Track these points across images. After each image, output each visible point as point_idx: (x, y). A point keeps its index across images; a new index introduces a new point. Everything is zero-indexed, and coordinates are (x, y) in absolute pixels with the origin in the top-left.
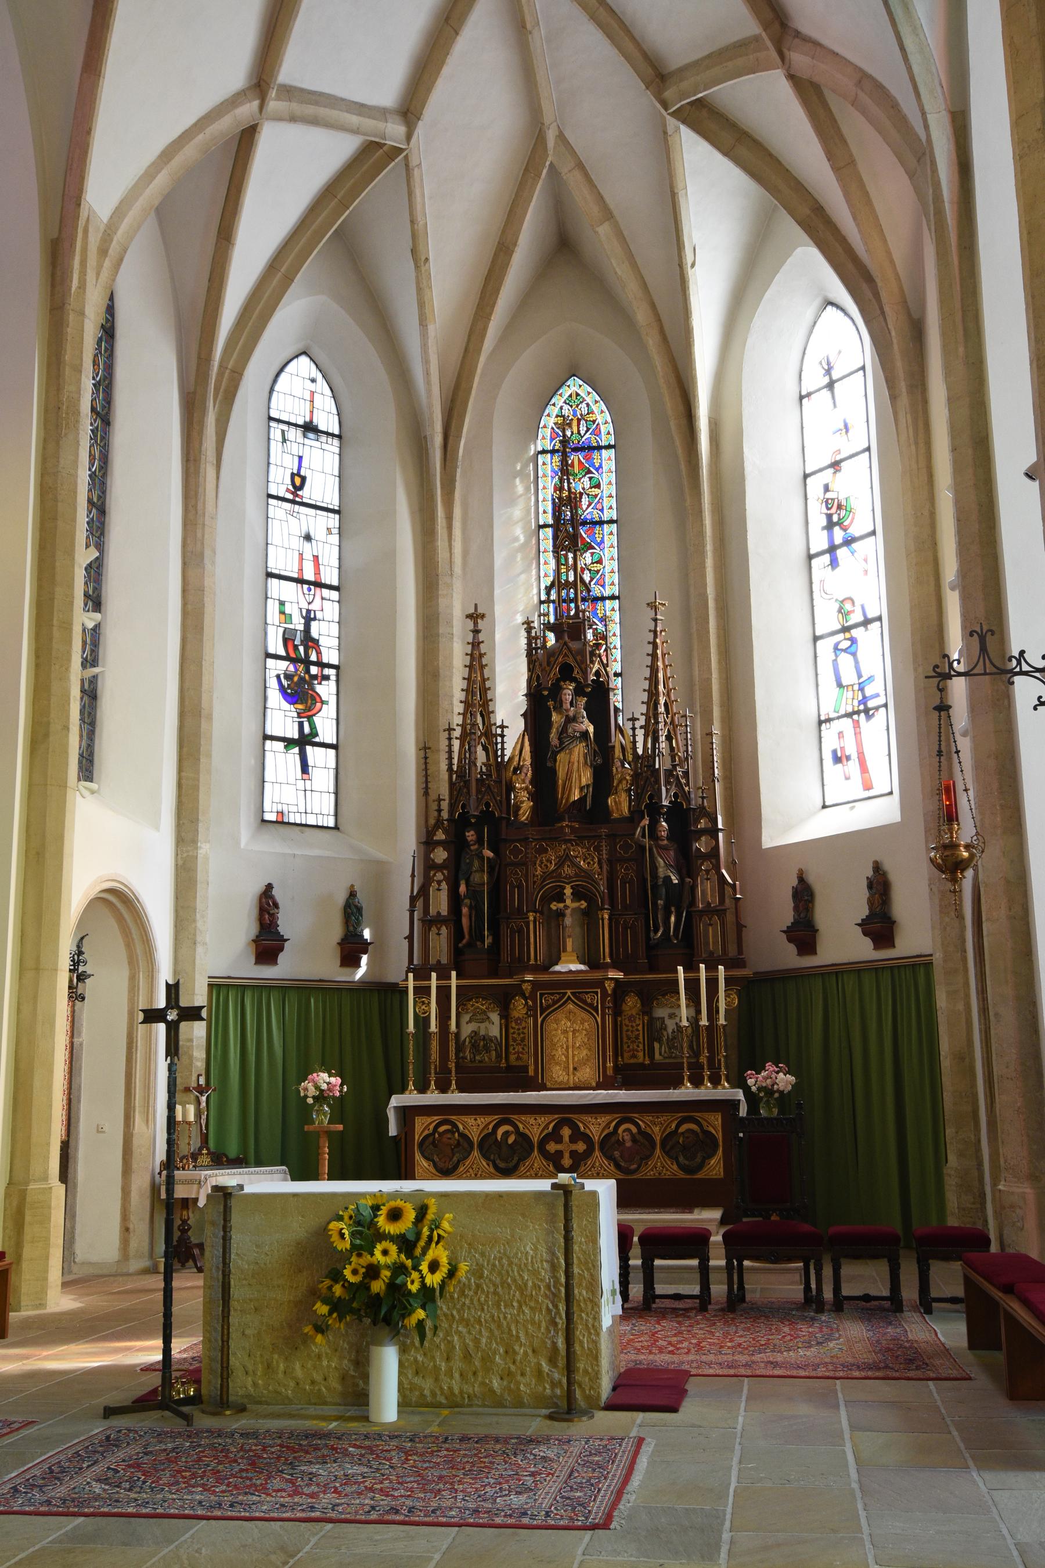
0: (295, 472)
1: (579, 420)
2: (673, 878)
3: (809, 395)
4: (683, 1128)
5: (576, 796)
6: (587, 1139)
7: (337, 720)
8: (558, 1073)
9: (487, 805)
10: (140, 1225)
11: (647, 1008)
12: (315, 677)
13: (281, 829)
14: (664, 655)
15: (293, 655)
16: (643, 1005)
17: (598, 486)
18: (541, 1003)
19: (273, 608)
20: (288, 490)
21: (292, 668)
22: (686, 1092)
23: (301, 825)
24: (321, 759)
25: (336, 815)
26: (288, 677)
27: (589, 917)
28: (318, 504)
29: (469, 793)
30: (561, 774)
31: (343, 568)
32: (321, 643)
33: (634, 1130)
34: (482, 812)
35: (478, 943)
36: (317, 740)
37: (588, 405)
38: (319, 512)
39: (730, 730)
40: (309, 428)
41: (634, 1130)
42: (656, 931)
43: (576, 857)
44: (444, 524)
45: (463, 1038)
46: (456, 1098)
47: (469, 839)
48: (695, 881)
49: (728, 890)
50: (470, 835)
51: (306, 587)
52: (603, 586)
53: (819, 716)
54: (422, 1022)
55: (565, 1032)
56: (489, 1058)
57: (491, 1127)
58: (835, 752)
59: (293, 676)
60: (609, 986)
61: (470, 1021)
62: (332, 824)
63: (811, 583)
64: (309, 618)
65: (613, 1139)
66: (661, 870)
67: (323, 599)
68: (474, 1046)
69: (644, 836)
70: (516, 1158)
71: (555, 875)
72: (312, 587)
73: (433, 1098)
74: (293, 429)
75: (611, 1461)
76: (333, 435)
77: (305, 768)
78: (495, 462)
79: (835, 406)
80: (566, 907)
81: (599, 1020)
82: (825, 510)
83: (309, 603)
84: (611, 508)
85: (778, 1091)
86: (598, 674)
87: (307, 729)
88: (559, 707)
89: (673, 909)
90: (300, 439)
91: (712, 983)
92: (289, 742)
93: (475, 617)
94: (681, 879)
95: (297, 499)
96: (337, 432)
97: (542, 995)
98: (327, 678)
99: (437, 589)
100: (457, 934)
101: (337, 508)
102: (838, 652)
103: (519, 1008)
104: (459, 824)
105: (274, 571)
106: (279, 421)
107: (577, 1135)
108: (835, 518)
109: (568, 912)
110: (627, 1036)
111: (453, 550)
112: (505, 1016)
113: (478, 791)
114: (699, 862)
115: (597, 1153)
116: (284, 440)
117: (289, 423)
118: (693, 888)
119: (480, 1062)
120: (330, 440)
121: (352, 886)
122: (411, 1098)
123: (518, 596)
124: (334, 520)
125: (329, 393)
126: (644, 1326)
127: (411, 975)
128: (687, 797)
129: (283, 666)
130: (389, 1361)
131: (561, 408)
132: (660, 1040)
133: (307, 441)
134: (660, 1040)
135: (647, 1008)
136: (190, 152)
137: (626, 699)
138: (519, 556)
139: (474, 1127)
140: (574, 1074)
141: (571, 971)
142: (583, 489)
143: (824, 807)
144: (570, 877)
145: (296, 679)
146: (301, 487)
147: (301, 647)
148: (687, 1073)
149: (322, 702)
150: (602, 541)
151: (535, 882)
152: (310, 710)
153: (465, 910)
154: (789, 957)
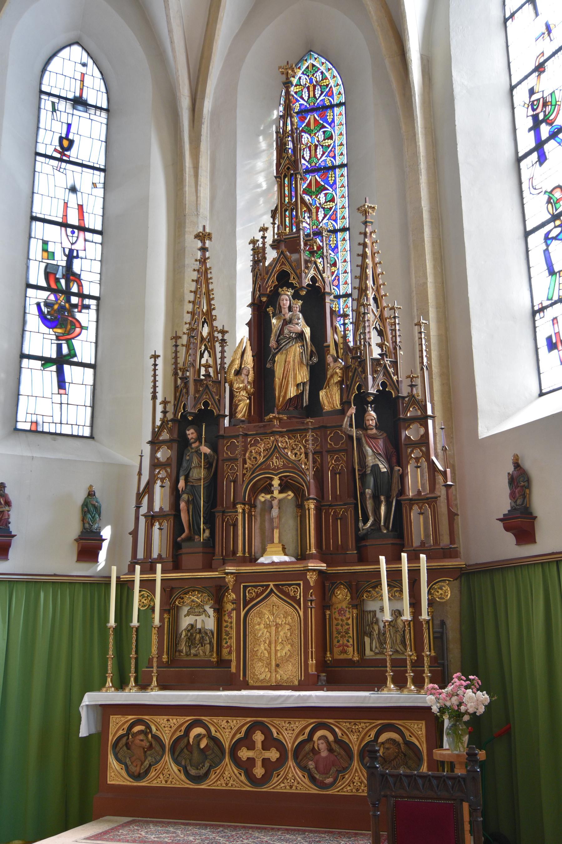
0: (64, 135)
1: (314, 87)
2: (381, 466)
3: (512, 16)
4: (383, 737)
5: (292, 392)
6: (280, 746)
7: (96, 343)
8: (260, 671)
9: (206, 404)
11: (357, 602)
12: (76, 306)
13: (32, 437)
14: (373, 254)
15: (53, 286)
16: (352, 598)
17: (331, 138)
18: (245, 596)
19: (36, 248)
20: (55, 150)
21: (52, 298)
22: (389, 696)
23: (55, 434)
24: (79, 378)
25: (92, 426)
26: (47, 304)
28: (84, 163)
29: (187, 393)
30: (279, 371)
31: (106, 216)
32: (82, 277)
33: (331, 738)
34: (200, 410)
35: (197, 537)
36: (75, 359)
37: (322, 73)
38: (84, 169)
39: (447, 329)
40: (79, 102)
41: (331, 738)
42: (365, 521)
43: (285, 448)
44: (192, 173)
45: (180, 632)
46: (156, 696)
47: (190, 437)
48: (404, 468)
49: (440, 478)
50: (191, 433)
51: (69, 230)
52: (336, 221)
53: (533, 306)
55: (268, 626)
57: (183, 728)
58: (549, 339)
59: (54, 304)
60: (312, 578)
61: (188, 614)
62: (87, 433)
63: (520, 183)
64: (71, 256)
65: (308, 747)
66: (370, 458)
67: (86, 240)
68: (190, 640)
69: (351, 426)
70: (207, 765)
71: (264, 466)
72: (76, 231)
73: (131, 696)
74: (63, 102)
76: (101, 109)
77: (62, 383)
78: (238, 122)
79: (537, 14)
80: (273, 498)
81: (301, 613)
82: (531, 113)
83: (72, 244)
84: (342, 154)
85: (466, 712)
86: (313, 279)
87: (65, 350)
88: (278, 312)
89: (382, 498)
90: (69, 110)
91: (414, 574)
92: (46, 361)
94: (391, 468)
95: (64, 158)
96: (105, 106)
97: (245, 587)
98: (88, 307)
99: (185, 227)
100: (178, 527)
101: (102, 167)
102: (549, 242)
105: (38, 215)
106: (49, 94)
107: (271, 742)
108: (541, 117)
109: (275, 503)
110: (337, 629)
112: (219, 611)
113: (197, 391)
114: (409, 450)
115: (291, 763)
116: (54, 110)
117: (59, 97)
118: (402, 477)
119: (195, 655)
120: (98, 112)
121: (91, 486)
122: (110, 696)
124: (99, 177)
125: (99, 76)
127: (138, 568)
128: (396, 386)
129: (43, 295)
131: (300, 78)
132: (370, 635)
133: (75, 112)
134: (370, 635)
135: (357, 602)
138: (261, 200)
139: (166, 728)
140: (276, 671)
141: (273, 563)
142: (318, 141)
143: (541, 394)
144: (279, 468)
145: (56, 307)
146: (69, 148)
147: (62, 279)
148: (390, 674)
149: (82, 328)
150: (335, 183)
151: (244, 475)
152: (68, 334)
153: (183, 505)
154: (507, 547)
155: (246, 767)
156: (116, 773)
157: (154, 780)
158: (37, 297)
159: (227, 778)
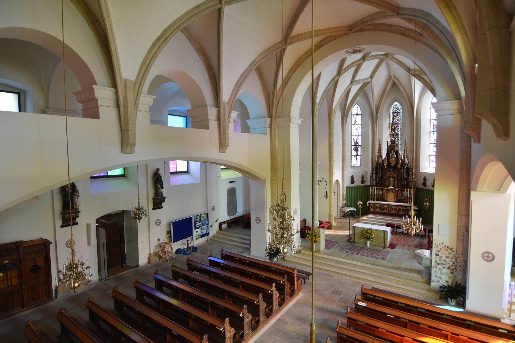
10: (339, 213)
27: (394, 181)
54: (372, 192)
56: (380, 196)
73: (373, 202)
75: (387, 253)
93: (380, 141)
100: (376, 181)
103: (384, 191)
104: (377, 168)
107: (391, 208)
111: (377, 129)
112: (382, 192)
122: (370, 202)
123: (386, 137)
126: (395, 236)
130: (369, 242)
136: (343, 95)
137: (401, 153)
139: (378, 206)
147: (356, 143)
154: (422, 187)
155: (388, 210)
156: (372, 209)
157: (376, 210)
158: (353, 147)
159: (385, 211)
